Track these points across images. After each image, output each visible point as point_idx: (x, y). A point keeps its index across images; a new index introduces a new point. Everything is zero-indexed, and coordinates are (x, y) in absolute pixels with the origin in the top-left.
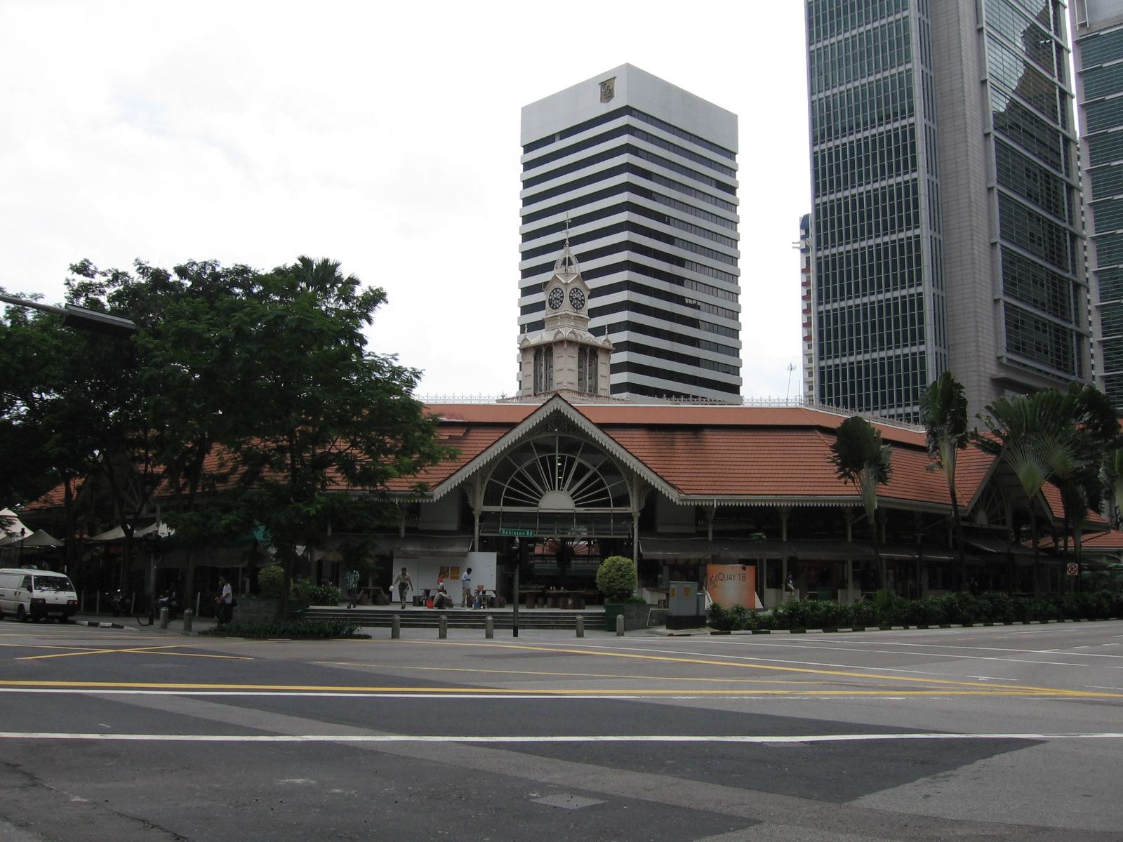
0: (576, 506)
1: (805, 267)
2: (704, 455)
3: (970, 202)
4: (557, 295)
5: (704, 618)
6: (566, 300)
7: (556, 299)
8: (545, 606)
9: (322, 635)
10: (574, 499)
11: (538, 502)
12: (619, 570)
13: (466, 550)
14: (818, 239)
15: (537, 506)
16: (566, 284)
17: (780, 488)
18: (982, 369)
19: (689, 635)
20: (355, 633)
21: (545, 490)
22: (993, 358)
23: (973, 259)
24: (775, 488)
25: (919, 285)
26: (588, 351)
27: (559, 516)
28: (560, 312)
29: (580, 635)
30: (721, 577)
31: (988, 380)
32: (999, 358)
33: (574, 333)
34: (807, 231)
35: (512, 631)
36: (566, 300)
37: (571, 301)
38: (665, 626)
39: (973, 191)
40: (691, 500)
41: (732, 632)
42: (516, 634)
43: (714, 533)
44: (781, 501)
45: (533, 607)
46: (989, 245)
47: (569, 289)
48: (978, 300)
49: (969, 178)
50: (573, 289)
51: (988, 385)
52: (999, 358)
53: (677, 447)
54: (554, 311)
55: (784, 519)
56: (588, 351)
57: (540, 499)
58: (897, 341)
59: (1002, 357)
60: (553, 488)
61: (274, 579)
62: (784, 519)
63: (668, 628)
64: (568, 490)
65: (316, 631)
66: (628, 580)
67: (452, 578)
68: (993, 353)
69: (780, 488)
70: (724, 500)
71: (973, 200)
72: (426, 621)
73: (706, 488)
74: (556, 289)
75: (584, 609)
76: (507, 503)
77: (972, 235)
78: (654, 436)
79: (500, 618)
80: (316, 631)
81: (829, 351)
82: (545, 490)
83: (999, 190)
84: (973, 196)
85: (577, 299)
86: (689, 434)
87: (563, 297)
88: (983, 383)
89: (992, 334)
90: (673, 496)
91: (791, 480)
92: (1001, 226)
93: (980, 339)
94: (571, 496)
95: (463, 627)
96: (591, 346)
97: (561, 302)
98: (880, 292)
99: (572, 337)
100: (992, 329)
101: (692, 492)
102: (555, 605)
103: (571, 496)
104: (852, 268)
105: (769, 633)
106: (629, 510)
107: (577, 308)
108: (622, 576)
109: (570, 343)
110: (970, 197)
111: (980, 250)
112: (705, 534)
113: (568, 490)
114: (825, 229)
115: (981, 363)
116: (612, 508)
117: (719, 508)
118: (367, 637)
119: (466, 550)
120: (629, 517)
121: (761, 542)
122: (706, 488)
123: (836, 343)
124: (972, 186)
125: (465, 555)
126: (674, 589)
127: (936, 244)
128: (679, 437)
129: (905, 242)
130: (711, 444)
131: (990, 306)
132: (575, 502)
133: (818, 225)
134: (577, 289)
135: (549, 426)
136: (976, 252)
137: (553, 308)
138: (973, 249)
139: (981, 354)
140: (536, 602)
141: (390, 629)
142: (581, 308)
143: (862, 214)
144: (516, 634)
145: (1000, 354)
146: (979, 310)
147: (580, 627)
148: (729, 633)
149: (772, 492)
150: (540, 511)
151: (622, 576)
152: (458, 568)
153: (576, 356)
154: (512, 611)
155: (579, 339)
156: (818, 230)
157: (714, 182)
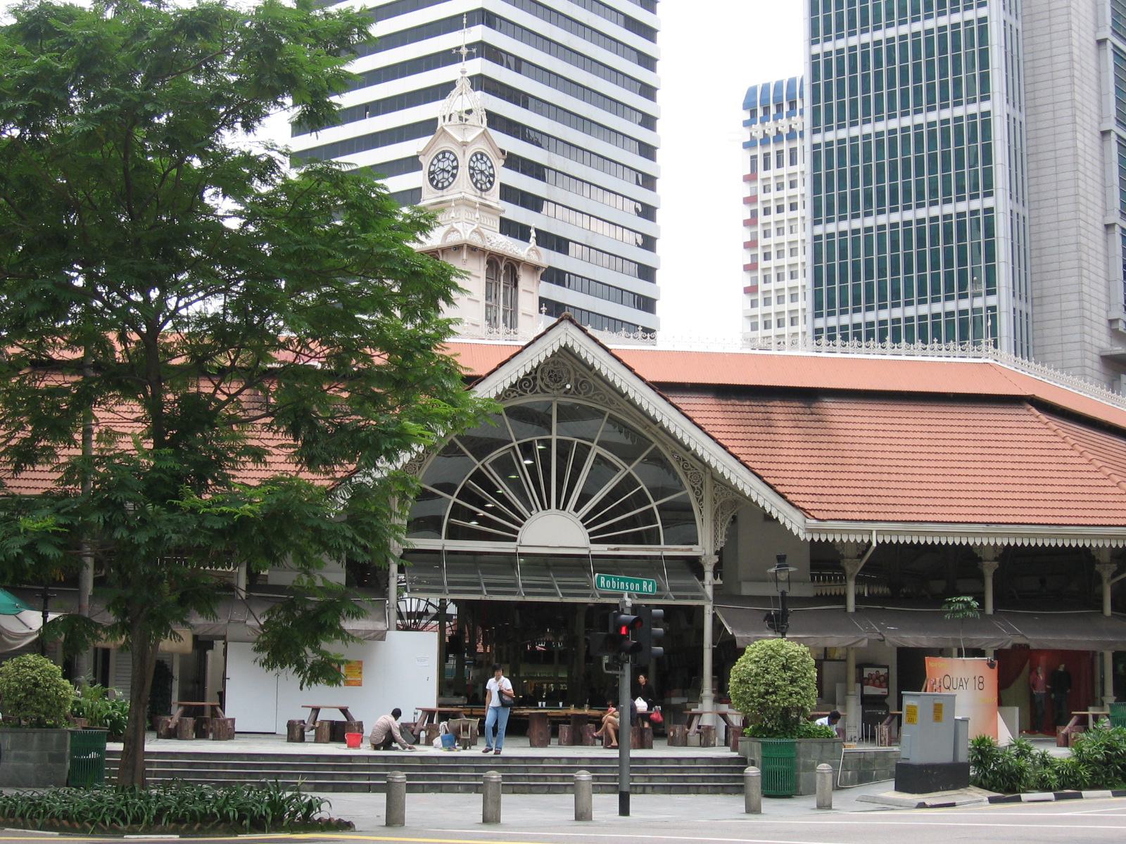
0: (592, 542)
1: (748, 172)
2: (832, 446)
3: (1072, 60)
4: (446, 165)
5: (965, 767)
6: (463, 173)
7: (443, 170)
8: (554, 741)
9: (246, 822)
10: (587, 527)
11: (516, 532)
12: (785, 668)
13: (381, 626)
14: (816, 112)
15: (515, 540)
16: (465, 144)
17: (992, 511)
18: (1087, 338)
19: (953, 805)
20: (324, 813)
21: (530, 509)
22: (1104, 322)
23: (1076, 155)
24: (985, 511)
25: (988, 194)
26: (502, 267)
27: (537, 559)
28: (450, 194)
29: (752, 809)
30: (947, 681)
31: (1096, 358)
32: (1111, 322)
33: (481, 234)
34: (753, 113)
35: (615, 798)
36: (463, 173)
37: (472, 176)
38: (892, 784)
39: (1075, 43)
40: (827, 531)
41: (1024, 796)
42: (624, 810)
43: (859, 598)
44: (995, 535)
45: (544, 744)
46: (1098, 134)
47: (470, 152)
48: (1082, 223)
49: (1070, 22)
50: (475, 154)
51: (1097, 366)
52: (1111, 322)
53: (781, 430)
54: (440, 193)
55: (989, 570)
56: (502, 267)
57: (520, 525)
58: (936, 290)
59: (1117, 320)
60: (546, 506)
61: (36, 685)
62: (989, 570)
63: (899, 788)
64: (577, 509)
65: (232, 813)
66: (804, 689)
67: (348, 683)
68: (1103, 313)
69: (992, 511)
70: (890, 532)
71: (1075, 58)
72: (369, 777)
73: (854, 508)
74: (444, 153)
75: (651, 747)
76: (454, 533)
77: (1074, 116)
78: (731, 408)
79: (457, 769)
80: (232, 813)
81: (831, 303)
82: (530, 509)
83: (1115, 46)
84: (1076, 51)
85: (482, 172)
86: (795, 407)
87: (456, 168)
88: (1088, 363)
89: (1102, 281)
90: (795, 523)
91: (1009, 496)
92: (1117, 104)
93: (1085, 289)
94: (583, 521)
95: (450, 789)
96: (509, 258)
97: (454, 176)
98: (920, 206)
99: (477, 241)
100: (1102, 273)
101: (830, 515)
102: (577, 740)
103: (583, 521)
104: (835, 170)
105: (1080, 797)
106: (695, 551)
107: (481, 189)
108: (793, 681)
109: (473, 249)
110: (1071, 53)
111: (1087, 141)
112: (842, 599)
113: (577, 509)
114: (828, 97)
115: (1087, 328)
116: (662, 546)
117: (882, 546)
118: (345, 826)
119: (381, 626)
120: (694, 566)
121: (970, 614)
122: (854, 508)
123: (843, 290)
124: (1074, 34)
125: (381, 636)
126: (912, 710)
127: (1013, 126)
128: (780, 412)
129: (938, 127)
130: (840, 426)
131: (1100, 231)
132: (591, 534)
133: (815, 89)
134: (482, 155)
135: (539, 382)
136: (1080, 145)
137: (436, 187)
138: (1075, 139)
139: (1087, 314)
140: (555, 733)
141: (381, 798)
142: (487, 190)
143: (891, 73)
144: (624, 810)
145: (1113, 316)
146: (1083, 240)
147: (755, 788)
148: (1018, 800)
149: (978, 519)
150: (521, 550)
151: (793, 681)
152: (360, 662)
153: (483, 274)
154: (618, 756)
155: (488, 246)
156: (815, 98)
157: (621, 18)
